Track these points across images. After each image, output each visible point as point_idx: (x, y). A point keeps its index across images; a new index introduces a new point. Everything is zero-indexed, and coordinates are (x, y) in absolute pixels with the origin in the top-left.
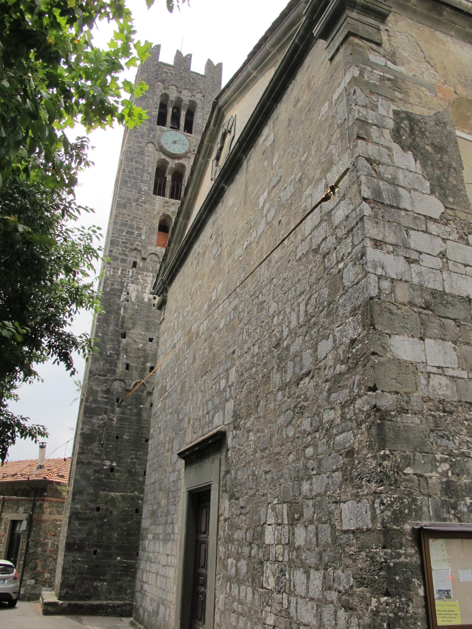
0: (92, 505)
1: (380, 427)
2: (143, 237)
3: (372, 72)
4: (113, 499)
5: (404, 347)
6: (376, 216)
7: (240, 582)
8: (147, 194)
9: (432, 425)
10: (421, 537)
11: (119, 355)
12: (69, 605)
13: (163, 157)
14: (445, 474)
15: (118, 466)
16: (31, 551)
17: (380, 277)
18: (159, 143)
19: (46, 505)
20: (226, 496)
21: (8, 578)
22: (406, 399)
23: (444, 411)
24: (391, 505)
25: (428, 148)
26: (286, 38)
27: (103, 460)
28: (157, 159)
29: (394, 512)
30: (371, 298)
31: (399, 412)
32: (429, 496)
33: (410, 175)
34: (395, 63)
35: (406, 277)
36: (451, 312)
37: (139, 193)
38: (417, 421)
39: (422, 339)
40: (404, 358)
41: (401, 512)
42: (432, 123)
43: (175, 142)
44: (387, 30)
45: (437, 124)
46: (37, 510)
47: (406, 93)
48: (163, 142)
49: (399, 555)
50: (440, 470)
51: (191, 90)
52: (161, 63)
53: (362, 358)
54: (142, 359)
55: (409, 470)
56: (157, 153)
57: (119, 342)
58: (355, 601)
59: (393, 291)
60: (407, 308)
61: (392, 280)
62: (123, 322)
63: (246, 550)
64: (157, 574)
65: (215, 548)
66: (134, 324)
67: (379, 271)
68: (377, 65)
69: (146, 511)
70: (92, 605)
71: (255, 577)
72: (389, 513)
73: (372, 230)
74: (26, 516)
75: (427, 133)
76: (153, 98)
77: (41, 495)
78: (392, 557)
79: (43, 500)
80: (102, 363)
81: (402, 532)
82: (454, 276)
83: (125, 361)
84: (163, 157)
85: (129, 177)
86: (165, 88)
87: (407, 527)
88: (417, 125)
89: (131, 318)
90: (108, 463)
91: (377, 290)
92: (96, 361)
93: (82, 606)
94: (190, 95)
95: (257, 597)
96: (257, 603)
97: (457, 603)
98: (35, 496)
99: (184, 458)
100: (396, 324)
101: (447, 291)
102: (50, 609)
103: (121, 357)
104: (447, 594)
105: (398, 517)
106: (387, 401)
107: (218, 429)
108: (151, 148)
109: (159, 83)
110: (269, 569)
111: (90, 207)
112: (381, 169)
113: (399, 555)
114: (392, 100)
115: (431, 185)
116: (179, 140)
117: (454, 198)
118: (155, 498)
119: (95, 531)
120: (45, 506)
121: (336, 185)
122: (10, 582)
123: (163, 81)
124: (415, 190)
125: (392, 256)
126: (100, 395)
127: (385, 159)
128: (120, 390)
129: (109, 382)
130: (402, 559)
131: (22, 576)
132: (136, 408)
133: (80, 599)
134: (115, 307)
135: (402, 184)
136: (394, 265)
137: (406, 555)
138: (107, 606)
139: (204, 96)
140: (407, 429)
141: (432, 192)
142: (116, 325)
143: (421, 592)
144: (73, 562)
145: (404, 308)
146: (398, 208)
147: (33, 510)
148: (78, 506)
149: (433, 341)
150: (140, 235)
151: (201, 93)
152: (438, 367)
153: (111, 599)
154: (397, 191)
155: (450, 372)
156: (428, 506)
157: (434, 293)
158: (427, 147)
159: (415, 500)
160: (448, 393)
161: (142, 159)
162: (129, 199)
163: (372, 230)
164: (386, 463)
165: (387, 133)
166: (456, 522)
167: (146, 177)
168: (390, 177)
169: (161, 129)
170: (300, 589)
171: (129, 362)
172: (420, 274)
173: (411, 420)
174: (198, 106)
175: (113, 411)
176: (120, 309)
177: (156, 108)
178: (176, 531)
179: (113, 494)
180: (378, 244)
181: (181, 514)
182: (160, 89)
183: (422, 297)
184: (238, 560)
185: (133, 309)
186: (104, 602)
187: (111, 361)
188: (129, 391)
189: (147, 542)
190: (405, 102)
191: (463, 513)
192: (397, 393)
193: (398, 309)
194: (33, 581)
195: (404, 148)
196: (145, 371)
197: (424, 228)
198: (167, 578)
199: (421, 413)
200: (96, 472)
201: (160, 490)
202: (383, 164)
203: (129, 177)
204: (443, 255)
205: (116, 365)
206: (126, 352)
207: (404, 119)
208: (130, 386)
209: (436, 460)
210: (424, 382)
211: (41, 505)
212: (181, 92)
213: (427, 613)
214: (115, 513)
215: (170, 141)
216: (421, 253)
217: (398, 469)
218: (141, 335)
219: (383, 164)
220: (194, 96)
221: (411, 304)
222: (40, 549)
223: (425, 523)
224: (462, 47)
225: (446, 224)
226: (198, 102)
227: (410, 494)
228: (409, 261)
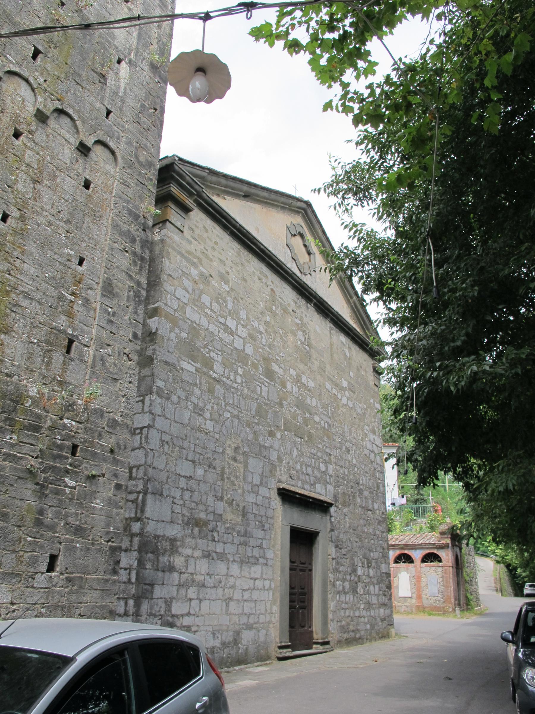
7: (345, 593)
26: (210, 209)
58: (386, 593)
63: (348, 577)
71: (354, 590)
92: (111, 292)
95: (355, 598)
96: (356, 601)
110: (360, 585)
111: (350, 139)
170: (372, 592)
181: (279, 543)
184: (344, 582)
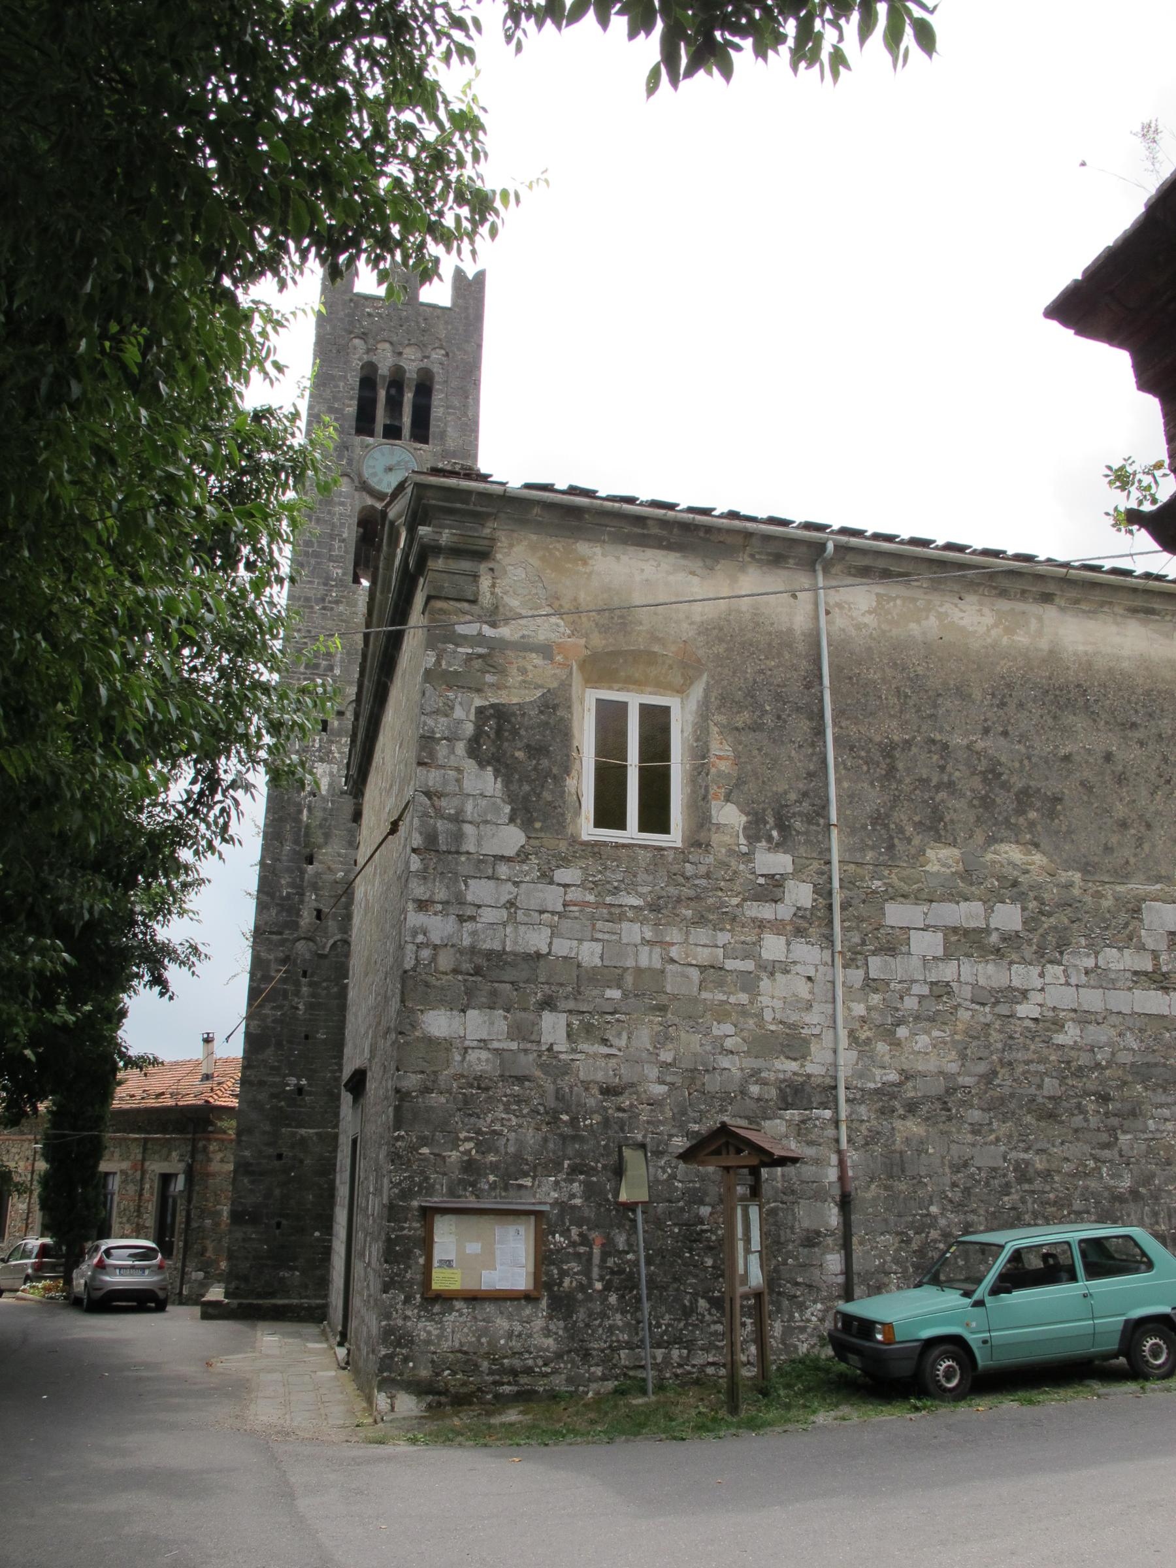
0: (270, 1151)
1: (397, 1109)
2: (337, 672)
4: (303, 1141)
5: (438, 1023)
6: (425, 869)
8: (341, 583)
10: (428, 1214)
11: (302, 895)
12: (240, 1305)
13: (370, 501)
15: (310, 1085)
16: (194, 1225)
18: (360, 475)
19: (213, 1147)
21: (148, 1267)
24: (400, 1183)
27: (285, 1076)
28: (357, 508)
33: (483, 803)
35: (455, 940)
36: (510, 974)
37: (325, 584)
38: (443, 1100)
39: (463, 1011)
41: (410, 1189)
43: (391, 470)
44: (492, 570)
45: (541, 712)
46: (199, 1157)
48: (366, 474)
49: (403, 1229)
50: (462, 1149)
51: (421, 346)
52: (358, 295)
55: (425, 1150)
56: (357, 495)
57: (302, 872)
59: (434, 959)
60: (450, 977)
61: (435, 947)
62: (307, 835)
66: (327, 836)
67: (420, 938)
70: (275, 1306)
74: (181, 1166)
76: (345, 377)
77: (205, 1131)
78: (394, 1230)
79: (209, 1140)
80: (274, 912)
81: (408, 1209)
83: (314, 905)
84: (370, 501)
85: (306, 554)
86: (368, 351)
87: (415, 1203)
89: (321, 826)
90: (293, 1080)
93: (259, 1307)
94: (419, 355)
97: (459, 1271)
98: (195, 1133)
102: (210, 1310)
103: (307, 899)
104: (448, 1264)
105: (406, 1195)
108: (344, 486)
109: (357, 341)
113: (403, 1229)
115: (512, 809)
116: (398, 463)
117: (544, 821)
119: (277, 1192)
120: (211, 1148)
122: (153, 1273)
123: (363, 336)
124: (486, 822)
125: (439, 918)
126: (273, 966)
127: (452, 788)
128: (308, 956)
129: (288, 944)
131: (184, 1266)
133: (259, 1296)
134: (292, 809)
135: (469, 818)
137: (410, 1229)
138: (300, 1307)
139: (447, 355)
142: (296, 842)
143: (421, 1261)
144: (244, 1240)
145: (445, 977)
146: (458, 853)
147: (193, 1157)
148: (247, 1153)
149: (476, 1012)
150: (331, 668)
151: (441, 348)
153: (306, 1297)
154: (460, 829)
155: (496, 1045)
156: (442, 1184)
157: (489, 954)
158: (517, 754)
159: (427, 1179)
160: (489, 1068)
161: (329, 512)
162: (307, 599)
164: (399, 1144)
165: (461, 748)
166: (473, 1199)
167: (338, 549)
169: (362, 441)
171: (321, 906)
172: (474, 933)
174: (437, 379)
175: (297, 993)
176: (300, 812)
177: (352, 398)
179: (303, 1131)
180: (422, 905)
182: (358, 354)
183: (471, 961)
185: (325, 809)
186: (295, 1301)
187: (290, 908)
188: (322, 957)
191: (482, 1190)
194: (201, 1275)
195: (482, 765)
199: (449, 1091)
200: (273, 1096)
203: (306, 554)
204: (511, 904)
205: (298, 915)
206: (315, 888)
208: (324, 947)
209: (458, 1139)
210: (458, 1058)
211: (205, 1148)
212: (400, 354)
214: (308, 1162)
215: (380, 469)
216: (479, 907)
218: (339, 855)
220: (428, 357)
221: (456, 971)
222: (208, 1222)
223: (435, 1201)
224: (618, 558)
225: (523, 862)
226: (436, 369)
227: (422, 1172)
228: (461, 919)
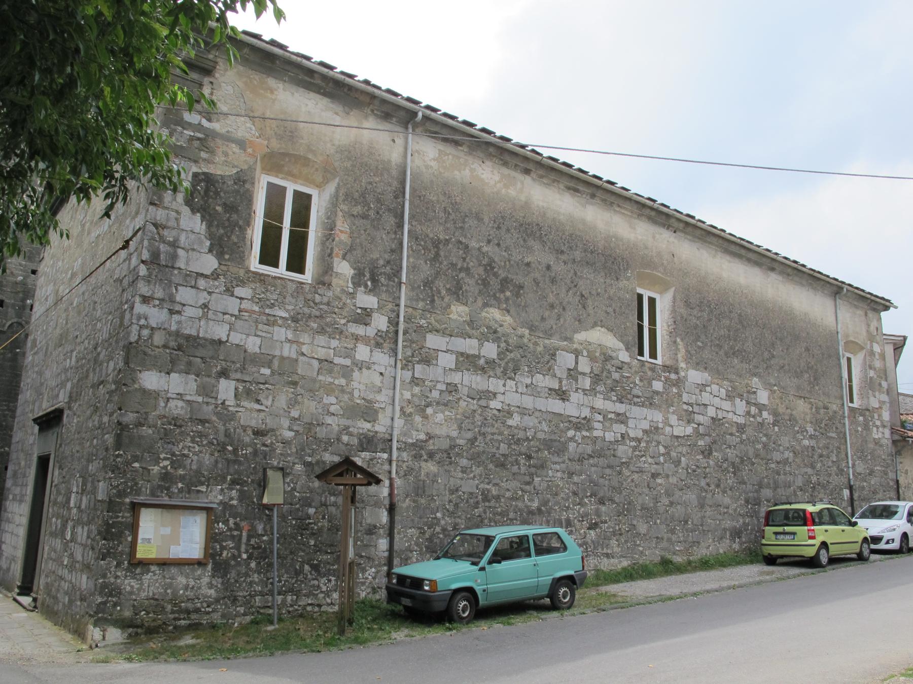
3: (182, 133)
5: (151, 380)
6: (150, 276)
9: (162, 435)
10: (135, 508)
14: (165, 467)
17: (141, 327)
20: (57, 465)
22: (144, 416)
23: (175, 425)
24: (117, 486)
25: (219, 208)
29: (119, 491)
30: (131, 343)
31: (136, 426)
32: (149, 481)
33: (193, 236)
34: (209, 120)
35: (166, 326)
36: (201, 352)
38: (150, 431)
39: (168, 373)
40: (149, 387)
41: (124, 491)
42: (230, 183)
44: (211, 83)
45: (235, 183)
47: (212, 152)
49: (118, 517)
50: (161, 465)
53: (124, 381)
54: (21, 295)
55: (136, 465)
60: (161, 350)
61: (152, 329)
64: (12, 533)
65: (49, 510)
67: (143, 322)
68: (190, 124)
69: (9, 473)
72: (115, 491)
73: (143, 288)
75: (222, 194)
78: (112, 518)
81: (123, 503)
82: (211, 323)
87: (127, 500)
88: (214, 186)
91: (137, 337)
99: (38, 424)
100: (148, 362)
101: (201, 335)
105: (121, 494)
106: (130, 418)
107: (56, 406)
112: (165, 233)
113: (118, 517)
114: (196, 162)
115: (211, 244)
117: (231, 255)
118: (18, 458)
121: (131, 239)
124: (193, 250)
125: (156, 309)
127: (172, 223)
130: (120, 519)
132: (11, 352)
135: (182, 246)
136: (156, 315)
140: (141, 437)
141: (210, 251)
145: (157, 350)
149: (177, 375)
152: (178, 394)
154: (176, 252)
155: (188, 398)
156: (146, 488)
157: (188, 338)
159: (136, 484)
160: (182, 412)
163: (143, 288)
165: (180, 197)
166: (167, 498)
168: (171, 239)
173: (146, 431)
178: (28, 493)
180: (146, 300)
183: (176, 341)
189: (8, 503)
190: (207, 161)
191: (173, 493)
192: (138, 412)
193: (153, 351)
195: (193, 211)
196: (24, 309)
197: (193, 283)
198: (17, 536)
201: (22, 450)
202: (168, 228)
204: (205, 306)
207: (201, 181)
209: (159, 458)
210: (162, 404)
213: (188, 564)
216: (184, 305)
217: (128, 463)
218: (21, 265)
219: (168, 228)
221: (165, 346)
223: (141, 499)
224: (293, 94)
225: (215, 279)
227: (134, 480)
228: (172, 312)
